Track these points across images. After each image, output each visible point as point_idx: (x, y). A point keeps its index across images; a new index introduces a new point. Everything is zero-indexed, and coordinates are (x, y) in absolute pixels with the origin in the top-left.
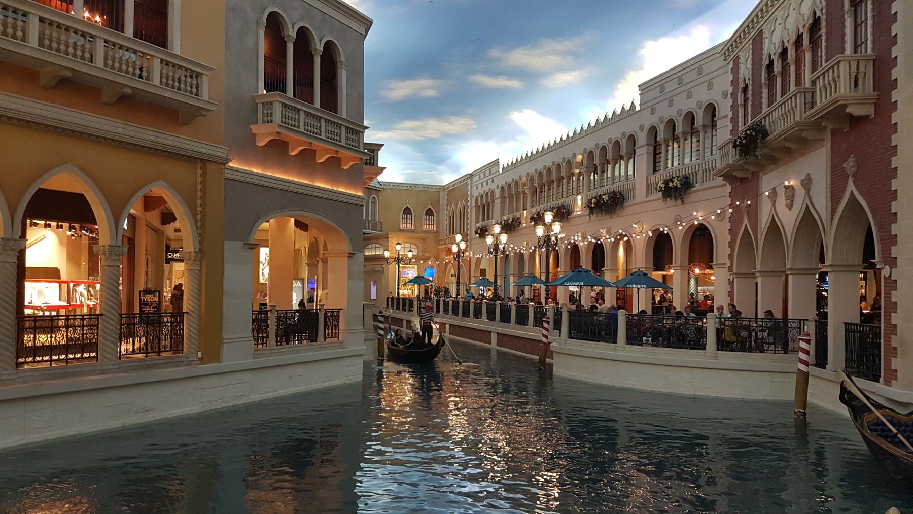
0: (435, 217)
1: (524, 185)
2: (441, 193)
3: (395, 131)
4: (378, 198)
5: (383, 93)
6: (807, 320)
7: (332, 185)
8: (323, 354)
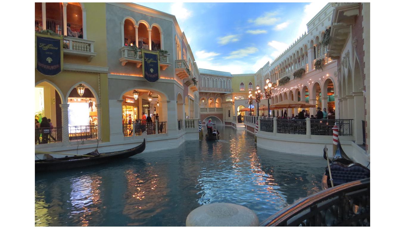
6: (353, 120)
7: (139, 75)
8: (157, 139)
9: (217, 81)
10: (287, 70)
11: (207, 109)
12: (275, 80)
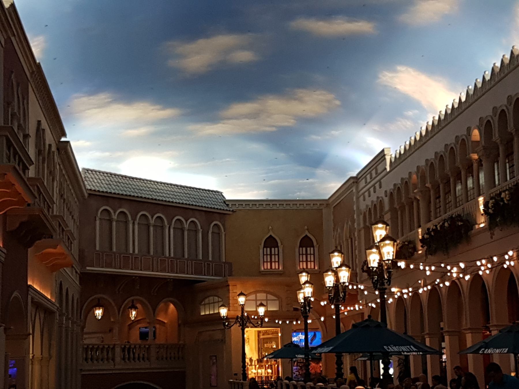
0: (316, 249)
1: (415, 186)
2: (324, 211)
3: (225, 121)
4: (224, 225)
5: (172, 63)
9: (162, 227)
10: (459, 187)
11: (113, 348)
12: (411, 230)
